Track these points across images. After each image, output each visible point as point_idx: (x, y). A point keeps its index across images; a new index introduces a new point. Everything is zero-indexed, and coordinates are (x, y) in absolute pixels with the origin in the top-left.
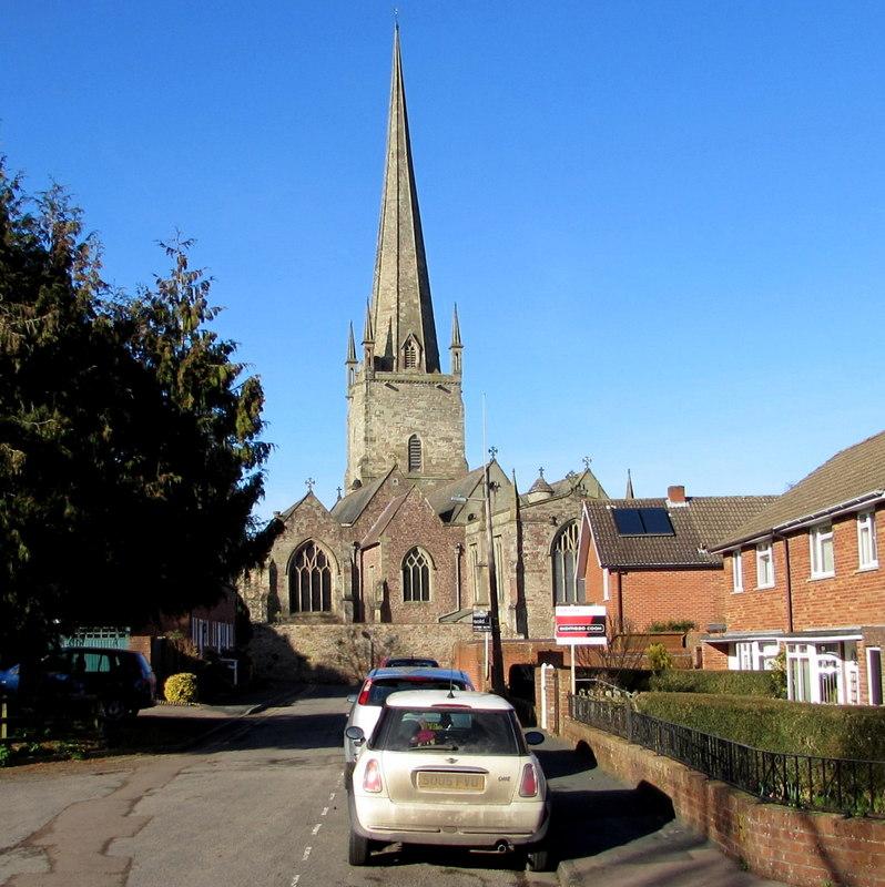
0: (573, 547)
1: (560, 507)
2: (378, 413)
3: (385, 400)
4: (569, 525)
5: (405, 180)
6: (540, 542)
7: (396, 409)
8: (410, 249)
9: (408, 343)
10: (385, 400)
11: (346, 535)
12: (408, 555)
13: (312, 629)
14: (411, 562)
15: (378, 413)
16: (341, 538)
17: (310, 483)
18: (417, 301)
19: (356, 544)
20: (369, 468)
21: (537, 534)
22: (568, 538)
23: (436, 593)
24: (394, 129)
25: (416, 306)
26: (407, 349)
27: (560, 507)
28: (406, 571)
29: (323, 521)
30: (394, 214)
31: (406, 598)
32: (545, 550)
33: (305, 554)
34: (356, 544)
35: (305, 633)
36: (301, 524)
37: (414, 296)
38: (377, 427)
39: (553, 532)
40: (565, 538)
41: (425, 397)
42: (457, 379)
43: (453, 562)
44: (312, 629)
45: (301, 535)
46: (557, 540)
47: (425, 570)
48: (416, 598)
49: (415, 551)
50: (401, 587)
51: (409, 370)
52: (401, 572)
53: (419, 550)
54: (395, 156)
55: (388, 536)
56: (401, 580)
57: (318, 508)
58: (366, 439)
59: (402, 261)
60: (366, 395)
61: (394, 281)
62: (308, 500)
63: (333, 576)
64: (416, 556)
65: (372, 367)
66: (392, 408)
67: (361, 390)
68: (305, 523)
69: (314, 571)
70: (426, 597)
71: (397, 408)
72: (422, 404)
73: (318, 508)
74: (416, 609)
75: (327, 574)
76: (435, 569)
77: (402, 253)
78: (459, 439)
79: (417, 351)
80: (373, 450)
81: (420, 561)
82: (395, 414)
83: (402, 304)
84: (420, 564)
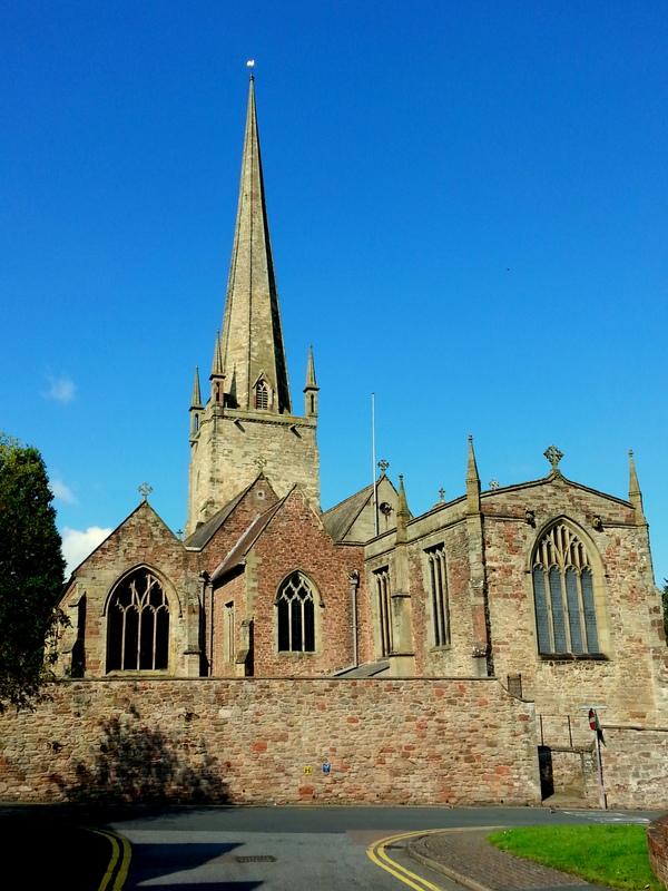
0: (562, 561)
1: (540, 498)
2: (226, 452)
3: (235, 439)
4: (554, 524)
5: (259, 221)
6: (514, 550)
7: (246, 449)
8: (263, 289)
9: (260, 382)
10: (235, 439)
11: (193, 562)
12: (285, 583)
13: (136, 689)
14: (290, 593)
15: (226, 452)
16: (185, 567)
17: (146, 490)
18: (270, 341)
19: (206, 575)
20: (146, 770)
21: (509, 537)
22: (553, 548)
23: (325, 640)
24: (248, 173)
25: (269, 346)
26: (259, 388)
27: (540, 498)
28: (282, 606)
29: (161, 541)
30: (247, 254)
31: (283, 646)
32: (520, 562)
33: (133, 585)
34: (206, 575)
35: (121, 696)
36: (130, 545)
37: (267, 337)
38: (225, 467)
39: (532, 536)
40: (549, 546)
41: (277, 440)
42: (313, 422)
43: (348, 596)
44: (136, 689)
45: (129, 560)
46: (538, 545)
47: (310, 606)
48: (297, 647)
49: (295, 578)
50: (275, 631)
51: (260, 411)
52: (276, 609)
53: (302, 578)
54: (249, 197)
55: (257, 554)
56: (275, 619)
57: (155, 524)
58: (212, 480)
59: (254, 300)
60: (214, 432)
61: (246, 319)
62: (141, 512)
63: (173, 618)
64: (296, 586)
65: (221, 403)
66: (242, 447)
67: (206, 430)
68: (136, 543)
69: (147, 613)
70: (310, 646)
71: (246, 449)
72: (275, 446)
73: (155, 524)
74: (295, 664)
75: (164, 616)
76: (323, 606)
77: (255, 292)
78: (313, 485)
79: (269, 392)
80: (220, 492)
81: (303, 593)
82: (246, 454)
83: (255, 344)
84: (290, 597)
